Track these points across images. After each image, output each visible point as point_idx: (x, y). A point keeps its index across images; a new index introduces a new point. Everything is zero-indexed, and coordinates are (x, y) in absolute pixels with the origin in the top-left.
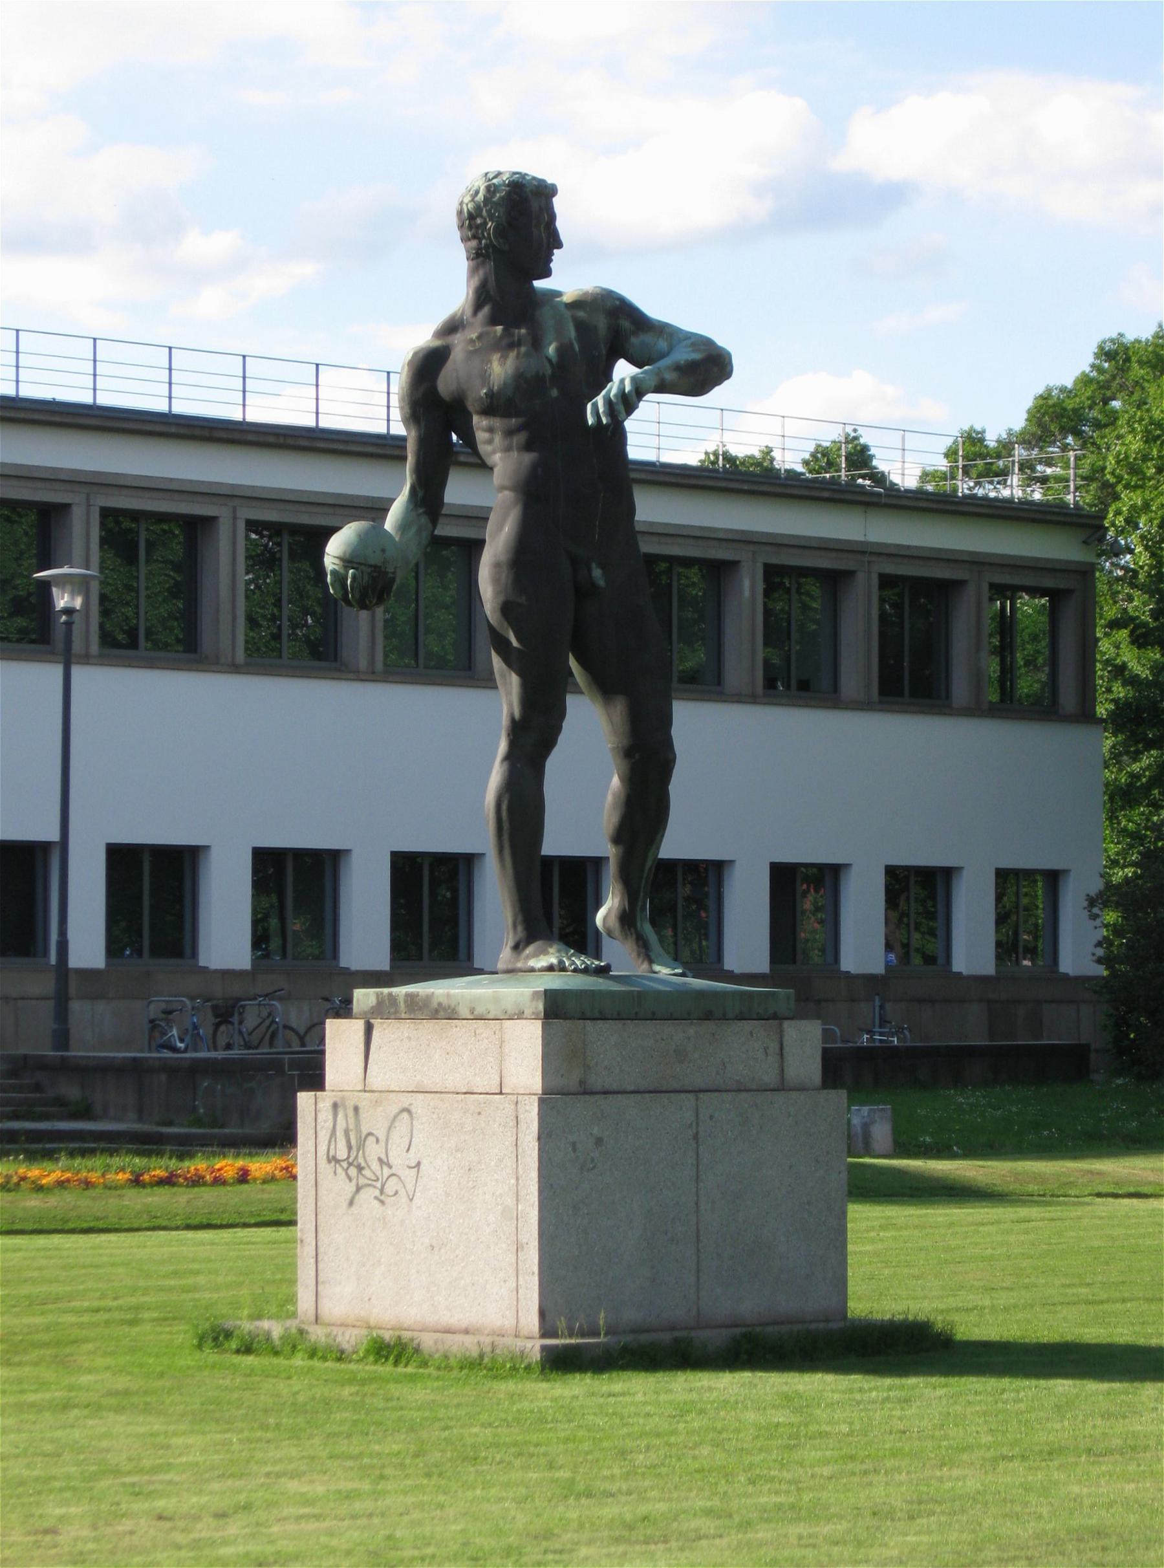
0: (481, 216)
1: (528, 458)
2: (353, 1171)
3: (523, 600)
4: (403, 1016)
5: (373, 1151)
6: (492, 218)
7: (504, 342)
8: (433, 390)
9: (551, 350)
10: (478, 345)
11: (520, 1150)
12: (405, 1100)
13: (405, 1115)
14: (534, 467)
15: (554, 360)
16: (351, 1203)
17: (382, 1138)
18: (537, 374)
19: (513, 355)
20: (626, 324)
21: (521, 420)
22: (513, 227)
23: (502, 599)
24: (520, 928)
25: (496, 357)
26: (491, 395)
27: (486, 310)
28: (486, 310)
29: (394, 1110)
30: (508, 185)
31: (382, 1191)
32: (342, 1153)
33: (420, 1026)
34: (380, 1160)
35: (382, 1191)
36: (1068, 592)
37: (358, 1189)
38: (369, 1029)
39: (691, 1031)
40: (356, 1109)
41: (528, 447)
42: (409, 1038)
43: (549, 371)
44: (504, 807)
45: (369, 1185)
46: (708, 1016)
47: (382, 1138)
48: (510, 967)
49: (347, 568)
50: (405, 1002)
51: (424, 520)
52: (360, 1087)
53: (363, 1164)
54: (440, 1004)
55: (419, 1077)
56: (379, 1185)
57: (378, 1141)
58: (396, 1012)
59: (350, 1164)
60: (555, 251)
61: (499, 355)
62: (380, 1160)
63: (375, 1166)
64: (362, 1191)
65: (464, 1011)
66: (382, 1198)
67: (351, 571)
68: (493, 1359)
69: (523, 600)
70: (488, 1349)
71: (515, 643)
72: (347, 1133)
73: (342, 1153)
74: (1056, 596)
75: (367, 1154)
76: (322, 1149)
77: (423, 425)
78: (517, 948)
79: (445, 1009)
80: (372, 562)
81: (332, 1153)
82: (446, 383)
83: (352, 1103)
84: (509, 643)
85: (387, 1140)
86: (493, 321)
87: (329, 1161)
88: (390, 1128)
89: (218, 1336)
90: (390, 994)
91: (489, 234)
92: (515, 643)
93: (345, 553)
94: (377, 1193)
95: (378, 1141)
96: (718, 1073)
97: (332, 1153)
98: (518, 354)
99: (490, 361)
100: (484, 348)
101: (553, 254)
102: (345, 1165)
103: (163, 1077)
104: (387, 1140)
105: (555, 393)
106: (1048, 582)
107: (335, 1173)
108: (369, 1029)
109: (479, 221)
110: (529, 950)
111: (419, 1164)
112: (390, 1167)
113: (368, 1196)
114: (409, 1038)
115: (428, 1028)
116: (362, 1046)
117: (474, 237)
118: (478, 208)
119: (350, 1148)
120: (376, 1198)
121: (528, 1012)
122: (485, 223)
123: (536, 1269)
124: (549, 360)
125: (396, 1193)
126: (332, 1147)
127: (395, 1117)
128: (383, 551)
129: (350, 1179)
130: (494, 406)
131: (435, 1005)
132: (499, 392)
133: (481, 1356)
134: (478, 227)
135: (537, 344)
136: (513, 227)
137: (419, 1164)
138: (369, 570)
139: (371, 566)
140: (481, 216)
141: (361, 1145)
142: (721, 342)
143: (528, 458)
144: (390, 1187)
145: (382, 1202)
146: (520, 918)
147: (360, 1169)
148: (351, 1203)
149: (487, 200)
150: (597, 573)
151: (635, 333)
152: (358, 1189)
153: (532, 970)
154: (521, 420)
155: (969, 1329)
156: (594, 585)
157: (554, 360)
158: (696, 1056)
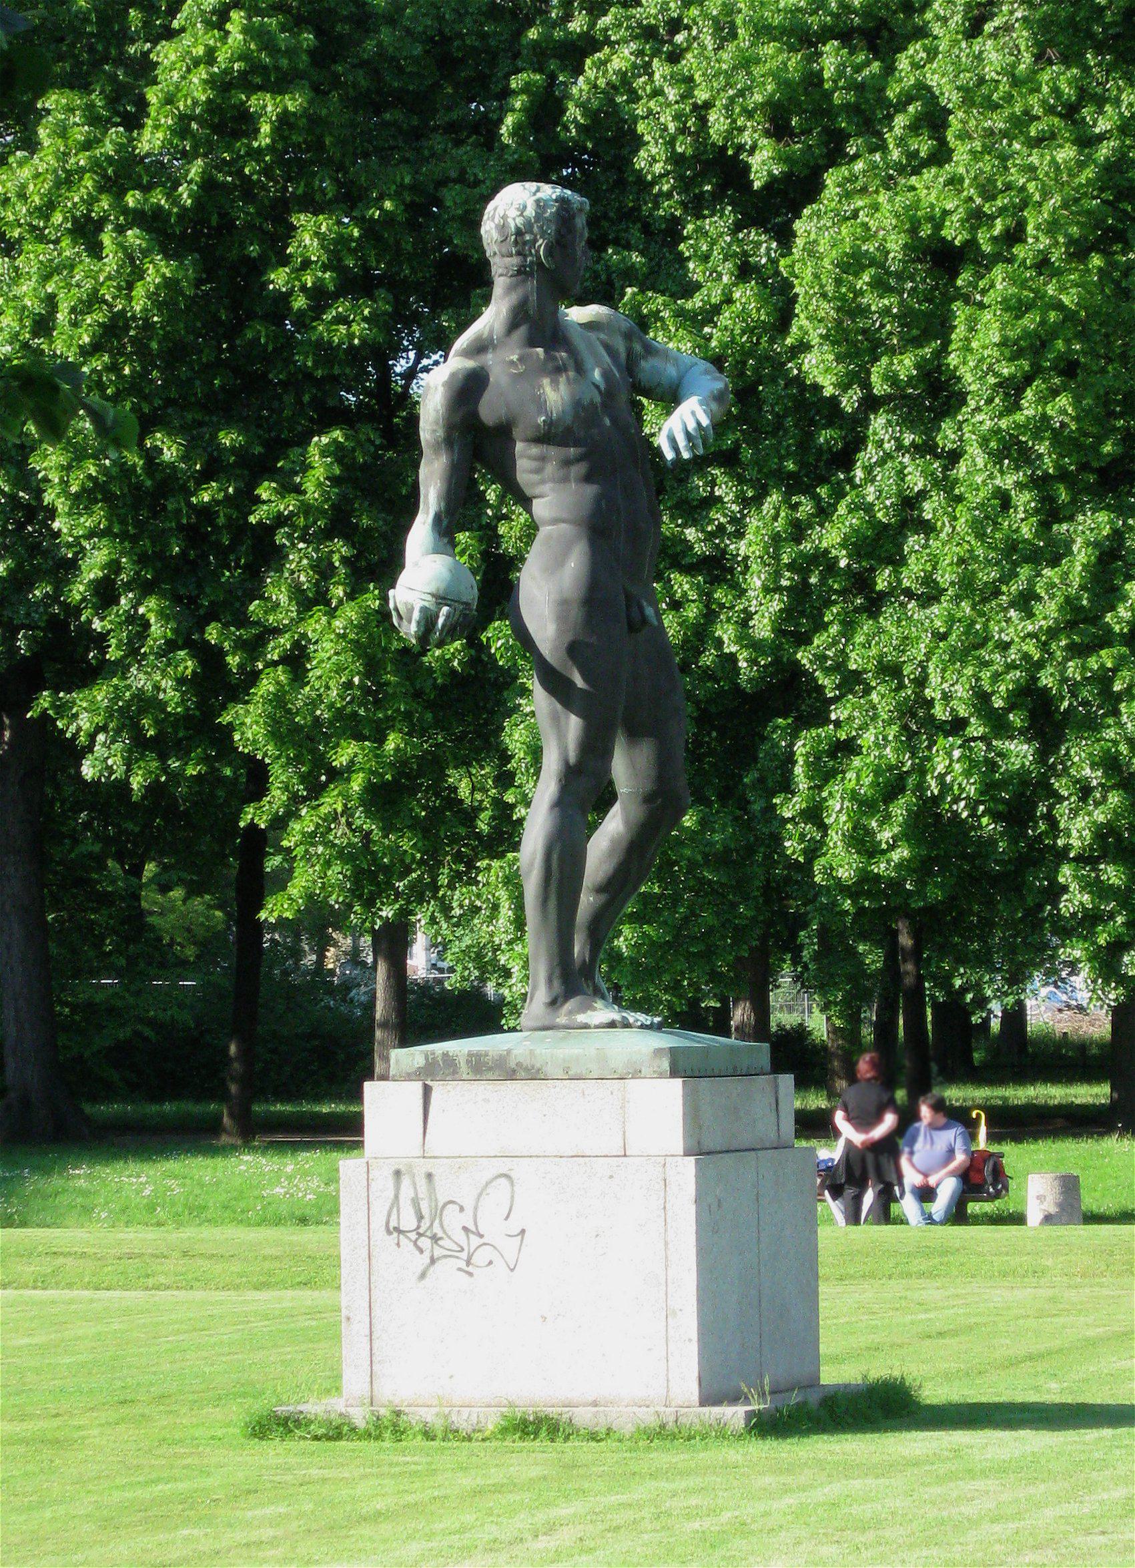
0: (531, 232)
1: (591, 490)
2: (425, 1243)
3: (593, 640)
4: (465, 1076)
5: (454, 1221)
6: (543, 234)
7: (550, 366)
8: (475, 414)
9: (597, 375)
10: (521, 368)
11: (669, 1214)
12: (502, 1166)
13: (503, 1181)
14: (598, 499)
16: (423, 1275)
17: (469, 1204)
19: (562, 379)
21: (579, 450)
23: (569, 638)
24: (557, 983)
25: (546, 381)
26: (550, 423)
27: (522, 331)
28: (522, 331)
29: (488, 1175)
30: (556, 201)
31: (468, 1263)
32: (408, 1221)
34: (465, 1229)
35: (468, 1263)
37: (433, 1261)
38: (427, 1091)
40: (429, 1176)
41: (588, 478)
43: (598, 399)
44: (555, 856)
45: (446, 1256)
47: (469, 1204)
48: (547, 1023)
49: (439, 605)
52: (420, 1153)
53: (440, 1234)
56: (464, 1255)
57: (462, 1209)
58: (455, 1072)
59: (420, 1235)
62: (465, 1229)
63: (460, 1237)
64: (438, 1265)
65: (550, 1070)
66: (470, 1269)
67: (445, 609)
68: (703, 1425)
69: (593, 640)
70: (672, 1418)
71: (579, 682)
72: (416, 1202)
73: (408, 1221)
75: (445, 1223)
76: (378, 1221)
77: (456, 448)
78: (554, 1003)
81: (393, 1224)
82: (489, 410)
83: (424, 1171)
84: (570, 683)
85: (476, 1208)
86: (532, 342)
87: (389, 1232)
88: (480, 1195)
89: (276, 1425)
91: (538, 251)
92: (579, 682)
93: (443, 586)
94: (463, 1265)
95: (462, 1209)
97: (393, 1224)
98: (568, 378)
99: (541, 386)
100: (529, 373)
102: (413, 1236)
104: (476, 1208)
105: (607, 422)
107: (398, 1245)
108: (427, 1091)
109: (528, 237)
110: (569, 1005)
111: (523, 1232)
112: (481, 1236)
113: (447, 1269)
117: (519, 253)
118: (529, 225)
119: (420, 1217)
120: (460, 1269)
122: (535, 241)
123: (694, 1335)
125: (491, 1263)
126: (394, 1217)
127: (487, 1184)
129: (421, 1251)
130: (547, 436)
131: (513, 1065)
132: (559, 419)
133: (663, 1426)
134: (525, 243)
135: (580, 369)
137: (523, 1232)
140: (531, 232)
141: (438, 1212)
143: (591, 490)
144: (480, 1257)
145: (470, 1274)
146: (557, 972)
147: (435, 1239)
148: (423, 1275)
149: (538, 217)
151: (644, 358)
152: (433, 1261)
153: (586, 1026)
154: (579, 450)
155: (932, 1394)
157: (602, 387)
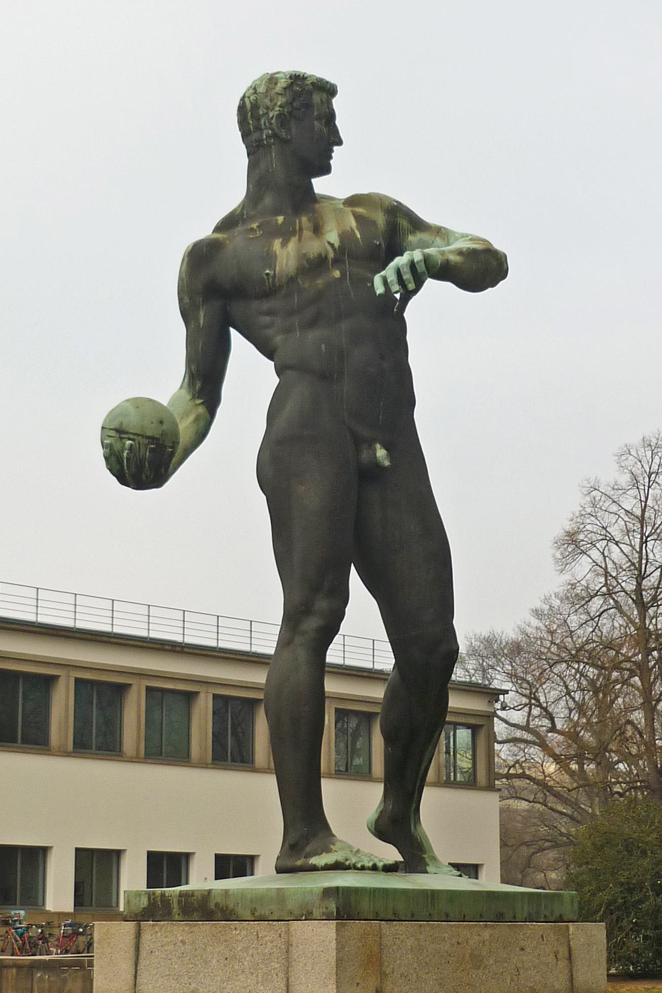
4: (177, 917)
15: (337, 245)
18: (320, 255)
20: (404, 223)
22: (291, 127)
33: (196, 929)
36: (481, 726)
39: (486, 934)
42: (183, 942)
43: (331, 255)
46: (499, 918)
50: (179, 902)
51: (201, 410)
54: (217, 905)
55: (193, 985)
60: (335, 148)
61: (281, 240)
74: (474, 729)
79: (222, 910)
80: (149, 434)
90: (163, 895)
96: (512, 980)
101: (332, 151)
103: (14, 970)
106: (472, 721)
114: (183, 942)
115: (206, 927)
116: (132, 950)
121: (316, 913)
124: (332, 245)
128: (161, 422)
136: (291, 127)
138: (146, 441)
139: (148, 437)
142: (498, 246)
150: (381, 453)
151: (413, 232)
153: (314, 868)
156: (377, 465)
157: (337, 245)
158: (491, 962)
